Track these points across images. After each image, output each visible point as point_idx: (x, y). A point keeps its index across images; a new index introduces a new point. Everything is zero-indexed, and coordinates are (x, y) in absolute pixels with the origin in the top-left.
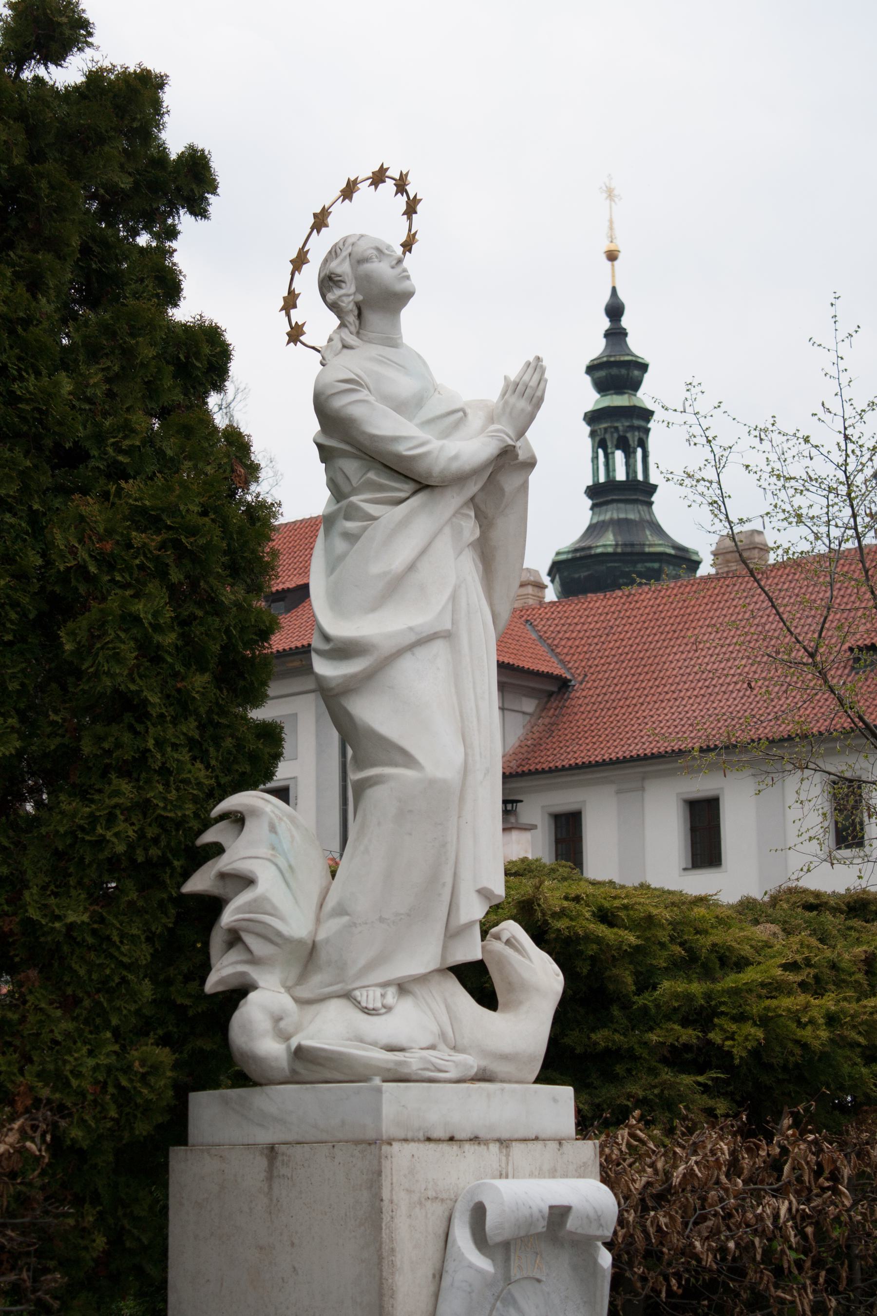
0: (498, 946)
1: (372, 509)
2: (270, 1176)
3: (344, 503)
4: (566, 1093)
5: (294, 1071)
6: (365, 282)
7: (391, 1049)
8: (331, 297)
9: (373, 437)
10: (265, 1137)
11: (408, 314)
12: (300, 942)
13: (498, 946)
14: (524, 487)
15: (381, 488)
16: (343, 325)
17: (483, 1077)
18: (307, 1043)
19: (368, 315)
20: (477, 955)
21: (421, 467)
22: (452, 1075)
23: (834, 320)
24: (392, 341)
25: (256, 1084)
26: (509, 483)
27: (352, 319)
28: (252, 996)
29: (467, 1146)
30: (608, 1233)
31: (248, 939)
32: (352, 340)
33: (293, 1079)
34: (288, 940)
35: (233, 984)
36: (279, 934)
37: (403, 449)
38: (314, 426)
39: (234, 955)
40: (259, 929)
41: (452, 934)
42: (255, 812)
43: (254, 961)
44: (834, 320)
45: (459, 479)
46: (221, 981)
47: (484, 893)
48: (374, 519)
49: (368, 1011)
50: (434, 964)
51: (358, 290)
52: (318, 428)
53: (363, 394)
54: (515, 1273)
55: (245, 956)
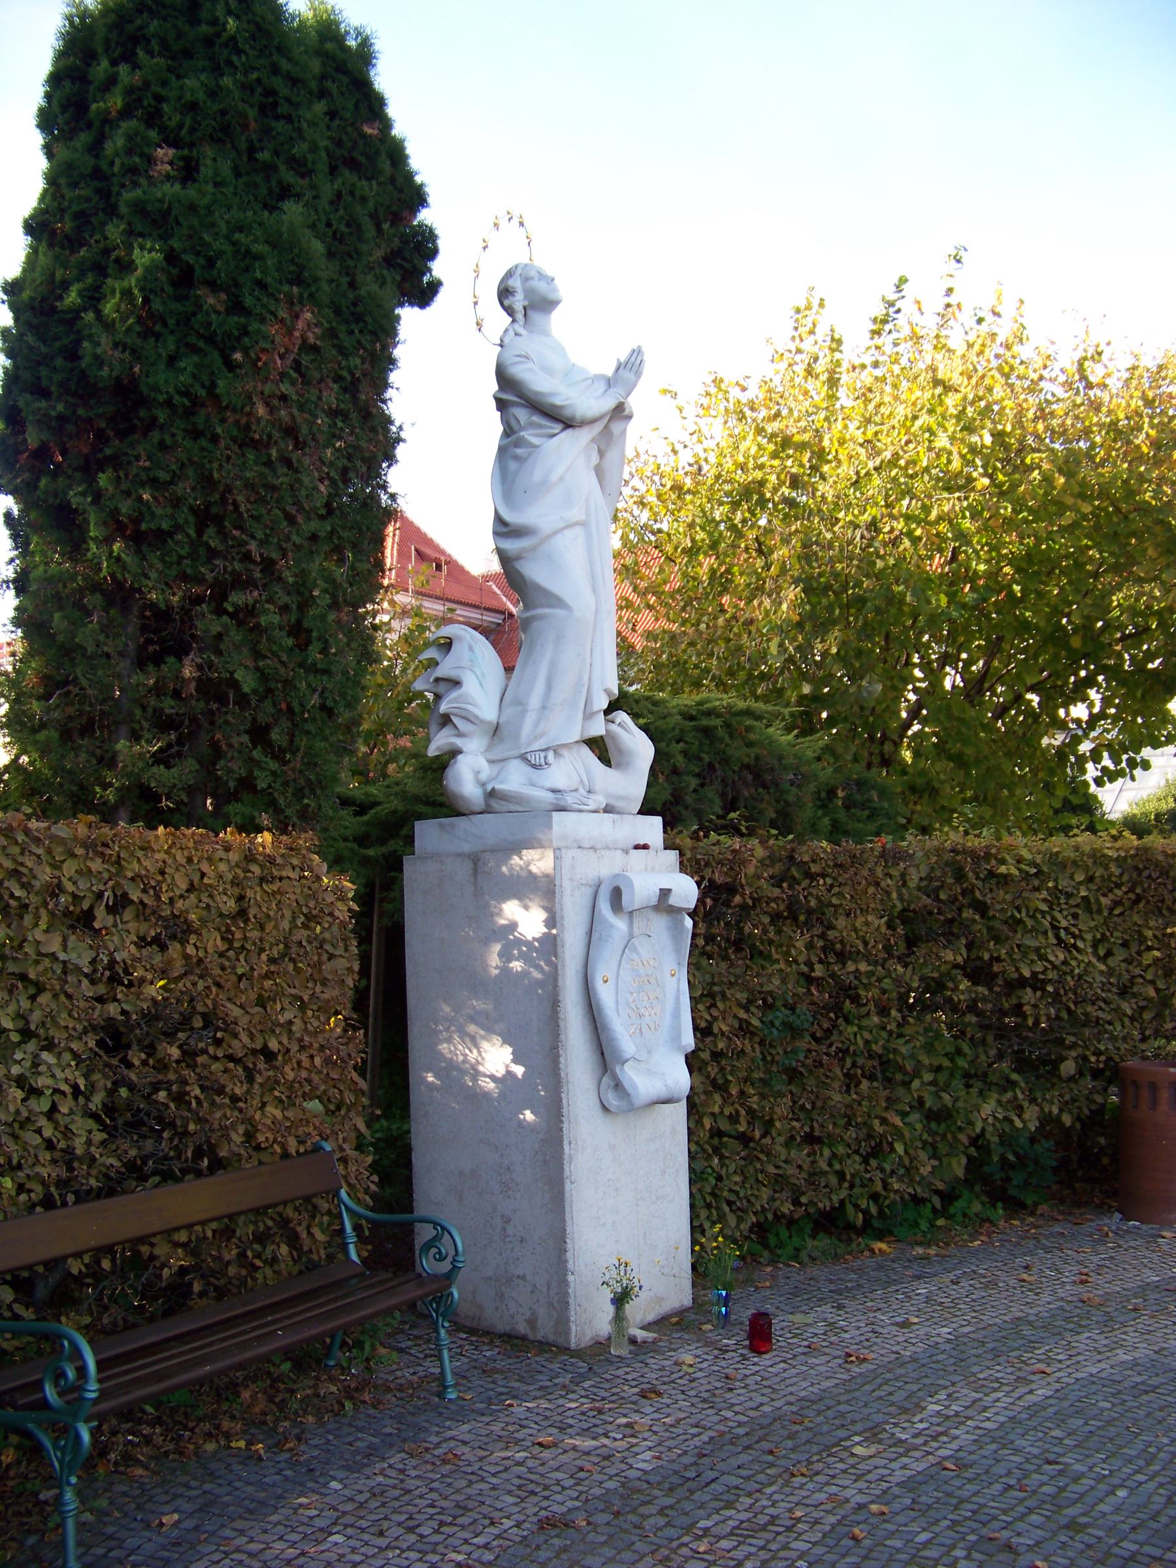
0: (613, 727)
1: (535, 440)
2: (475, 872)
3: (513, 437)
4: (657, 821)
5: (488, 805)
6: (530, 293)
7: (554, 791)
8: (506, 303)
9: (537, 393)
10: (466, 848)
11: (556, 315)
12: (489, 723)
13: (613, 727)
14: (624, 432)
15: (541, 427)
16: (514, 321)
17: (608, 809)
18: (498, 787)
19: (529, 312)
20: (603, 732)
21: (567, 413)
22: (592, 807)
23: (953, 300)
24: (546, 333)
25: (460, 814)
26: (616, 427)
27: (520, 316)
28: (460, 757)
29: (603, 852)
30: (692, 905)
31: (454, 719)
32: (521, 330)
33: (487, 810)
34: (482, 722)
35: (447, 748)
36: (476, 717)
37: (557, 401)
38: (494, 387)
39: (446, 731)
40: (463, 714)
41: (588, 716)
42: (460, 639)
43: (460, 735)
44: (953, 300)
45: (593, 421)
46: (438, 748)
47: (608, 692)
48: (536, 447)
49: (534, 766)
50: (577, 737)
51: (525, 298)
52: (496, 387)
53: (530, 365)
54: (636, 931)
55: (454, 732)
